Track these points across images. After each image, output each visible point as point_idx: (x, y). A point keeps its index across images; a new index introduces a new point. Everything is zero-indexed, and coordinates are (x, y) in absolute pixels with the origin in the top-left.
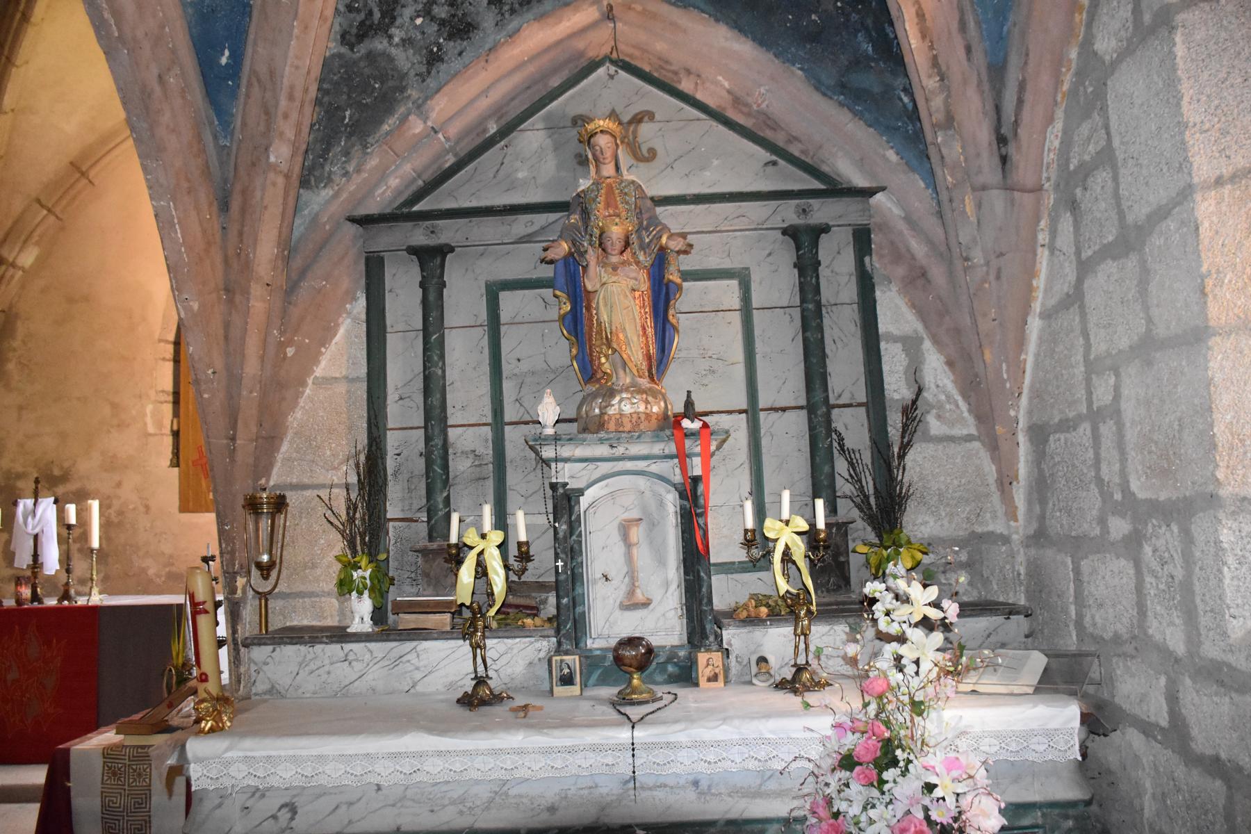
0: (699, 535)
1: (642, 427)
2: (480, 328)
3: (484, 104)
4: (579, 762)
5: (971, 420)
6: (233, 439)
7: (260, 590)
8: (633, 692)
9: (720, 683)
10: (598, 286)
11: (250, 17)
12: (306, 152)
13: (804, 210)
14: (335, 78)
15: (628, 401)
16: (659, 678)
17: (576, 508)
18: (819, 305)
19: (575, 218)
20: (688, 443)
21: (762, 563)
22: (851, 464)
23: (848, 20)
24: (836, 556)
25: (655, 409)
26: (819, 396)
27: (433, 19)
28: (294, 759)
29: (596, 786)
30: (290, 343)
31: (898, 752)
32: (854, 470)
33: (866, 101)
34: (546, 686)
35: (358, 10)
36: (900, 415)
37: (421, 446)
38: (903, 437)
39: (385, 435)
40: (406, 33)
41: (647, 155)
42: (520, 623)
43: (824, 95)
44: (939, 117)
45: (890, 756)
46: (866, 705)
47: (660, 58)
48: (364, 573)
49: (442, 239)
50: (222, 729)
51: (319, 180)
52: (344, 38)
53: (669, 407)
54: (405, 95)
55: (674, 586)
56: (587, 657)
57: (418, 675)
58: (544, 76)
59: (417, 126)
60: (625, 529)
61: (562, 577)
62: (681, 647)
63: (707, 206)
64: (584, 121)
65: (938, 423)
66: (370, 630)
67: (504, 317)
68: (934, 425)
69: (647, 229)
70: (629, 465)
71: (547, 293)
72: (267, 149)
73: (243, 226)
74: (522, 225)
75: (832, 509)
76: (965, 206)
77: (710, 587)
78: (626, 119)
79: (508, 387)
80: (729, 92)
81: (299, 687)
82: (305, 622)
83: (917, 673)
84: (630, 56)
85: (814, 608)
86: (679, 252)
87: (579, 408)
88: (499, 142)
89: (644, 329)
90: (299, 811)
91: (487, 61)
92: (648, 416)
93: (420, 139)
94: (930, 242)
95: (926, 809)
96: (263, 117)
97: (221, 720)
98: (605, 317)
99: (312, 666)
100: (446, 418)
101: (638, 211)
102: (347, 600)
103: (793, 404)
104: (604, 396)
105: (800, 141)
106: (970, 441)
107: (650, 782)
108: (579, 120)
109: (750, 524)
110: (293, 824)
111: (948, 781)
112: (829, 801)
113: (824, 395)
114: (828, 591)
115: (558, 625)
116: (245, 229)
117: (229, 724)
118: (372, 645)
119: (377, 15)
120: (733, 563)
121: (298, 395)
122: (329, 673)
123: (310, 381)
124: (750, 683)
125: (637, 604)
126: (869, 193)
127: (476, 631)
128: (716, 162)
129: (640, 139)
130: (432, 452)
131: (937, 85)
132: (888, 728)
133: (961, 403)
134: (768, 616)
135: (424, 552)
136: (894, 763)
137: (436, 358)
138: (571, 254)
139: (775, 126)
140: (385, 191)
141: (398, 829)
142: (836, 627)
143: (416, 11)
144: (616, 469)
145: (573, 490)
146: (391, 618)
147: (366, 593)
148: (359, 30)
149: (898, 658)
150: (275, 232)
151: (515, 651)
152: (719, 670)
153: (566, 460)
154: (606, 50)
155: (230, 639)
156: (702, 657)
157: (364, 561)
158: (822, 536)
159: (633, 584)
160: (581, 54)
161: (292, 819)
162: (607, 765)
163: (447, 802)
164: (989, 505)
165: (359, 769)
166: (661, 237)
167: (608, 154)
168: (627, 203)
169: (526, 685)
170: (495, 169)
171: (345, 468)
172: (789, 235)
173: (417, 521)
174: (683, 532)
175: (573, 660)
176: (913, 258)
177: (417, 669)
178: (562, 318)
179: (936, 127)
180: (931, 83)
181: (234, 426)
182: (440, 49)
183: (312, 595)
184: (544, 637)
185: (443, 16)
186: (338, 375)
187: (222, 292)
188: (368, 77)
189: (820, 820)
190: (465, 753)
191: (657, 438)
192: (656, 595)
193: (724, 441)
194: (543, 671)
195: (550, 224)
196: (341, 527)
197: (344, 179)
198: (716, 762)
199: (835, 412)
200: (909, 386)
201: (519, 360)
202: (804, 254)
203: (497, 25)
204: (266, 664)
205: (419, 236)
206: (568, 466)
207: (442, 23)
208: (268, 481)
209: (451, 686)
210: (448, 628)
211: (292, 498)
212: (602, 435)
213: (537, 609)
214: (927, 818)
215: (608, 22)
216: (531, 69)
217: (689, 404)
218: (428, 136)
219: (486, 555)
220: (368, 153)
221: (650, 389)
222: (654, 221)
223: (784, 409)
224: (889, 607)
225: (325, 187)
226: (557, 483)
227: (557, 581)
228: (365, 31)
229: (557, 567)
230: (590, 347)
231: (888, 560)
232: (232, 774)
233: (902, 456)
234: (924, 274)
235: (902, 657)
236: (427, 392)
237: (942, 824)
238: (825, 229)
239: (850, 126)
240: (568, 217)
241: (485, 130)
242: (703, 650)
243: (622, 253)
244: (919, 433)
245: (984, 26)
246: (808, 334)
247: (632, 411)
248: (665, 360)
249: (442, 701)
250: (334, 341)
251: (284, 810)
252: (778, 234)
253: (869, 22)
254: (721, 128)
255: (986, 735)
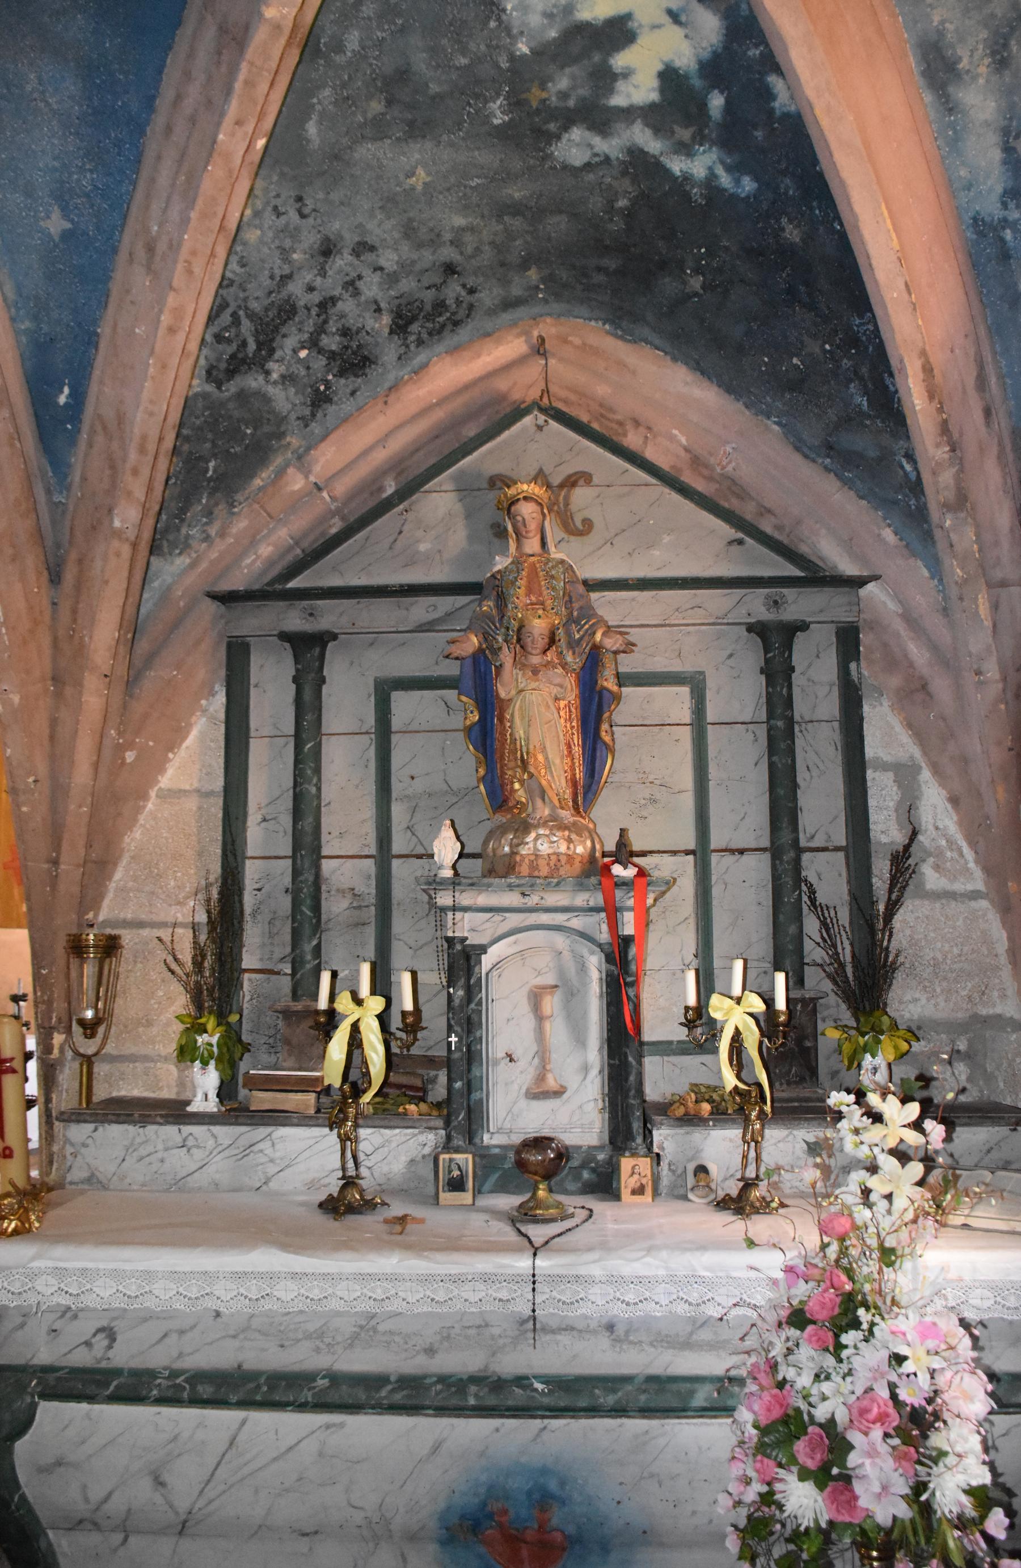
0: (627, 1010)
1: (562, 872)
2: (367, 737)
3: (380, 456)
4: (465, 1295)
5: (978, 873)
6: (56, 862)
7: (82, 1051)
8: (538, 1206)
9: (648, 1197)
10: (513, 692)
11: (97, 348)
12: (159, 513)
13: (776, 602)
14: (198, 422)
15: (546, 839)
16: (571, 1186)
17: (477, 969)
18: (791, 722)
19: (488, 606)
20: (619, 894)
21: (708, 1045)
22: (824, 924)
23: (839, 367)
24: (799, 1041)
25: (580, 850)
26: (786, 837)
27: (320, 351)
28: (116, 1275)
29: (487, 1325)
30: (130, 746)
31: (861, 1312)
32: (827, 930)
33: (858, 467)
34: (430, 1189)
35: (229, 341)
36: (888, 863)
37: (287, 880)
38: (890, 891)
39: (244, 863)
40: (287, 369)
41: (581, 527)
42: (401, 1110)
43: (806, 456)
44: (950, 495)
45: (850, 1316)
46: (824, 1247)
47: (601, 405)
48: (210, 1039)
49: (323, 624)
50: (29, 1231)
51: (173, 545)
52: (210, 374)
53: (598, 847)
54: (284, 442)
55: (594, 1071)
56: (483, 1157)
57: (272, 1169)
58: (455, 423)
59: (296, 482)
60: (536, 998)
61: (456, 1056)
62: (600, 1148)
63: (653, 593)
64: (503, 481)
65: (937, 875)
66: (215, 1110)
67: (396, 723)
68: (931, 877)
69: (577, 622)
70: (545, 918)
71: (451, 694)
72: (110, 511)
73: (77, 602)
74: (421, 609)
75: (795, 981)
76: (977, 606)
77: (640, 1075)
78: (556, 481)
79: (398, 811)
80: (687, 450)
81: (124, 1177)
82: (136, 1093)
83: (889, 1212)
84: (565, 401)
85: (768, 1108)
86: (616, 653)
87: (486, 843)
88: (398, 505)
89: (569, 746)
90: (119, 1338)
91: (386, 403)
92: (570, 858)
93: (296, 503)
94: (934, 648)
95: (892, 1387)
96: (108, 472)
97: (28, 1220)
98: (521, 732)
99: (143, 1151)
100: (319, 847)
101: (567, 598)
102: (187, 1068)
103: (753, 846)
104: (517, 831)
105: (774, 515)
106: (975, 899)
107: (554, 1324)
108: (499, 482)
109: (692, 1000)
110: (111, 1354)
111: (921, 1352)
112: (774, 1367)
113: (792, 836)
114: (789, 1083)
115: (449, 1115)
116: (81, 606)
117: (37, 1225)
118: (217, 1129)
119: (252, 346)
120: (670, 1043)
121: (138, 810)
122: (162, 1161)
123: (153, 794)
124: (685, 1198)
125: (547, 1092)
126: (860, 582)
127: (346, 1119)
128: (666, 539)
129: (573, 507)
130: (300, 890)
131: (946, 456)
132: (851, 1278)
133: (966, 850)
134: (712, 1113)
135: (287, 1014)
136: (856, 1324)
137: (309, 772)
138: (480, 651)
139: (742, 493)
140: (254, 561)
141: (239, 1367)
142: (795, 1132)
143: (300, 342)
144: (527, 923)
145: (473, 946)
146: (243, 1092)
147: (212, 1063)
148: (229, 364)
149: (866, 1192)
150: (117, 613)
151: (394, 1145)
152: (647, 1181)
153: (465, 909)
154: (534, 394)
155: (42, 1100)
156: (626, 1163)
157: (211, 1023)
158: (782, 1018)
159: (544, 1067)
160: (502, 398)
161: (110, 1347)
162: (500, 1300)
163: (300, 1336)
164: (997, 981)
165: (195, 1289)
166: (594, 633)
167: (533, 526)
168: (554, 589)
169: (405, 1187)
170: (391, 539)
171: (192, 903)
172: (758, 634)
173: (278, 973)
174: (609, 1005)
175: (465, 1160)
176: (911, 665)
177: (272, 1161)
178: (468, 730)
179: (947, 507)
180: (941, 453)
181: (57, 846)
182: (327, 388)
183: (146, 1058)
184: (430, 1128)
185: (334, 347)
186: (187, 787)
187: (50, 682)
188: (239, 421)
189: (762, 1388)
190: (325, 1276)
191: (581, 886)
192: (572, 1081)
193: (664, 893)
194: (426, 1170)
195: (457, 610)
196: (184, 978)
197: (204, 545)
198: (635, 1304)
199: (806, 857)
200: (901, 828)
201: (413, 778)
202: (774, 656)
203: (399, 358)
204: (85, 1145)
205: (295, 621)
206: (467, 915)
207: (332, 356)
208: (96, 915)
209: (312, 1185)
210: (312, 1111)
211: (128, 938)
212: (512, 880)
213: (424, 1090)
214: (894, 1396)
215: (538, 357)
216: (439, 415)
217: (623, 842)
218: (309, 494)
219: (362, 1027)
220: (234, 514)
221: (575, 824)
222: (588, 612)
223: (742, 852)
224: (858, 1125)
225: (180, 554)
226: (454, 938)
227: (449, 1059)
228: (237, 365)
229: (449, 1044)
230: (502, 767)
231: (865, 1049)
232: (39, 1288)
233: (890, 915)
234: (924, 687)
235: (870, 1191)
236: (297, 814)
237: (913, 1406)
238: (803, 626)
239: (837, 496)
240: (481, 602)
241: (381, 489)
242: (627, 1154)
243: (545, 652)
244: (911, 887)
245: (1008, 381)
246: (775, 759)
247: (551, 851)
248: (594, 787)
249: (303, 1204)
250: (184, 745)
251: (100, 1336)
252: (742, 631)
253: (864, 370)
254: (676, 497)
255: (977, 1284)
